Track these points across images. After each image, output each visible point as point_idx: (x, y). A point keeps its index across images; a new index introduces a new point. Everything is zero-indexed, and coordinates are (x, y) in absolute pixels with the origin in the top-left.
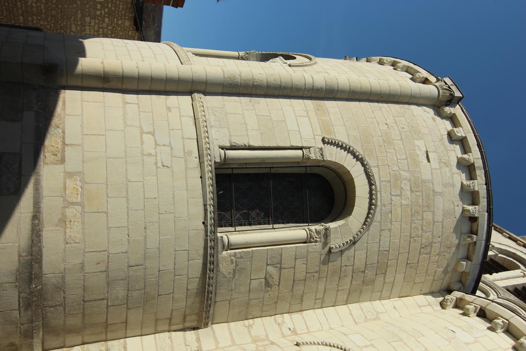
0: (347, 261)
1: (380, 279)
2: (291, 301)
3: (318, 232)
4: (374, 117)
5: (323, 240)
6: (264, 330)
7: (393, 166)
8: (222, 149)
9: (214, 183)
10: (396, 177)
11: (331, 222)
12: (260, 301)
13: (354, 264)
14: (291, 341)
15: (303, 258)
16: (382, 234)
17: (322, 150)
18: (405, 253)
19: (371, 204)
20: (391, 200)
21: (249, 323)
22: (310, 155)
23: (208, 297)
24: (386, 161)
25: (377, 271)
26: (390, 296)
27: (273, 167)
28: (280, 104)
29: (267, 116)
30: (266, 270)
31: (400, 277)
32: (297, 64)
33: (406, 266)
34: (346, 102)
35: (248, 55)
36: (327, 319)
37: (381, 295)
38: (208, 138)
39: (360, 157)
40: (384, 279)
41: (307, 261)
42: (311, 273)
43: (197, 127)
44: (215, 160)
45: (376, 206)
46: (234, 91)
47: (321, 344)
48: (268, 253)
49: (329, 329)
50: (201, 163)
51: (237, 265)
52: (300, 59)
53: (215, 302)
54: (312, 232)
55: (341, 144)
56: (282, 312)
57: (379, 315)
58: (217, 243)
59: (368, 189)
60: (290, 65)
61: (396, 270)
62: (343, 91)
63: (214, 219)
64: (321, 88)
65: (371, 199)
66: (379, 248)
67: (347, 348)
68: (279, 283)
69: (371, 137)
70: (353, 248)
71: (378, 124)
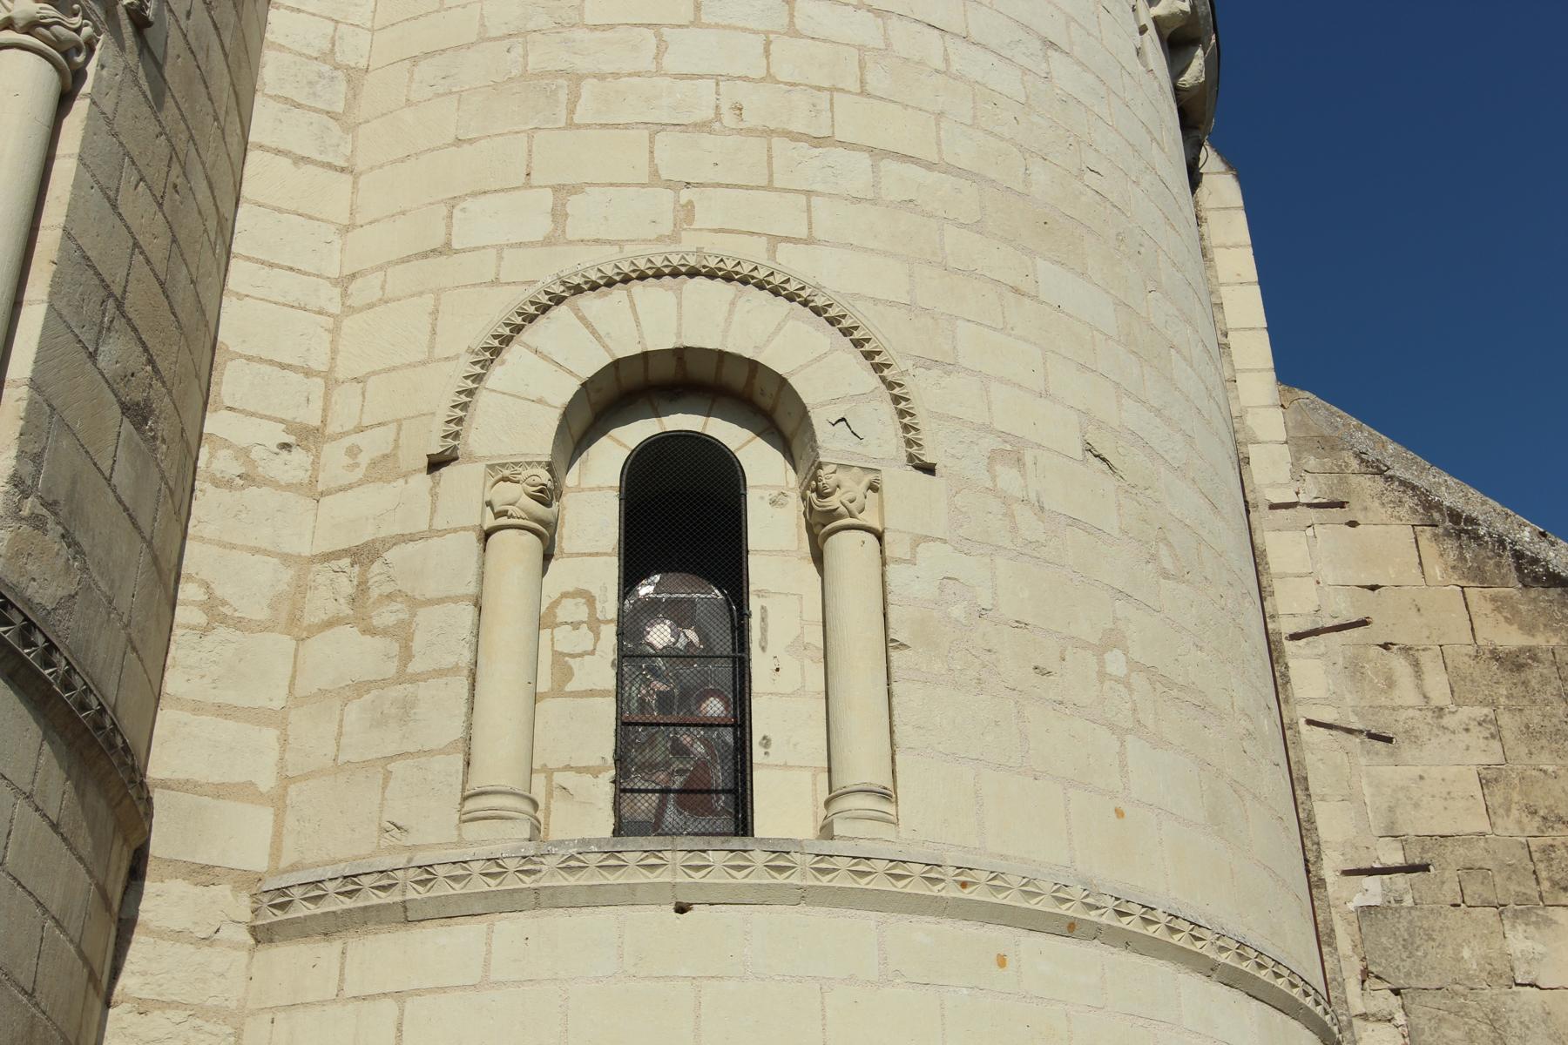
21: (193, 603)
36: (291, 269)
54: (47, 26)
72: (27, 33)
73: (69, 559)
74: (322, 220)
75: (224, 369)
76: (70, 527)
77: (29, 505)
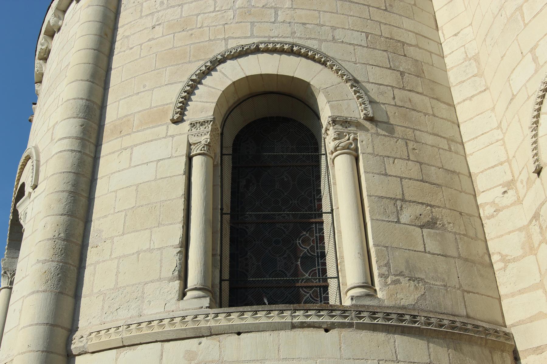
0: (386, 96)
1: (411, 51)
2: (456, 189)
3: (339, 136)
4: (140, 46)
5: (352, 129)
6: (511, 234)
7: (226, 17)
8: (184, 294)
9: (250, 310)
10: (245, 13)
11: (319, 118)
12: (461, 239)
13: (390, 86)
14: (529, 183)
15: (384, 162)
16: (339, 40)
17: (194, 124)
18: (369, 11)
19: (291, 52)
20: (283, 22)
21: (498, 261)
22: (203, 142)
23: (461, 329)
24: (218, 27)
25: (399, 54)
26: (437, 42)
27: (222, 209)
28: (106, 194)
29: (126, 215)
30: (408, 224)
31: (407, 24)
32: (32, 180)
33: (390, 12)
34: (110, 89)
35: (7, 272)
36: (483, 134)
37: (436, 54)
38: (161, 320)
39: (209, 64)
40: (411, 45)
41: (389, 157)
42: (408, 152)
43: (139, 343)
44: (207, 307)
45: (293, 45)
46: (73, 275)
47: (535, 131)
48: (377, 220)
49: (500, 130)
50: (211, 333)
51: (401, 274)
52: (27, 178)
53: (468, 317)
54: (338, 146)
55: (186, 93)
56: (475, 207)
57: (469, 56)
58: (364, 306)
59: (265, 55)
60: (34, 187)
61: (396, 27)
62: (91, 92)
63: (319, 311)
64: (82, 126)
65: (282, 51)
66: (364, 47)
67: (543, 87)
68: (428, 205)
69: (176, 49)
70: (363, 84)
71: (153, 39)
72: (336, 151)
73: (415, 285)
74: (485, 111)
75: (476, 181)
76: (411, 275)
77: (389, 279)
